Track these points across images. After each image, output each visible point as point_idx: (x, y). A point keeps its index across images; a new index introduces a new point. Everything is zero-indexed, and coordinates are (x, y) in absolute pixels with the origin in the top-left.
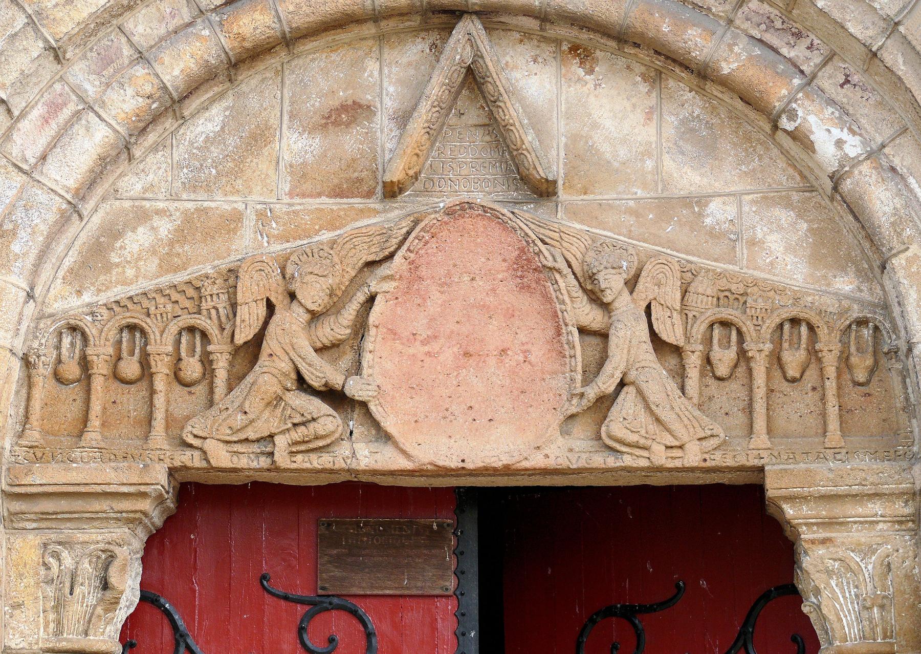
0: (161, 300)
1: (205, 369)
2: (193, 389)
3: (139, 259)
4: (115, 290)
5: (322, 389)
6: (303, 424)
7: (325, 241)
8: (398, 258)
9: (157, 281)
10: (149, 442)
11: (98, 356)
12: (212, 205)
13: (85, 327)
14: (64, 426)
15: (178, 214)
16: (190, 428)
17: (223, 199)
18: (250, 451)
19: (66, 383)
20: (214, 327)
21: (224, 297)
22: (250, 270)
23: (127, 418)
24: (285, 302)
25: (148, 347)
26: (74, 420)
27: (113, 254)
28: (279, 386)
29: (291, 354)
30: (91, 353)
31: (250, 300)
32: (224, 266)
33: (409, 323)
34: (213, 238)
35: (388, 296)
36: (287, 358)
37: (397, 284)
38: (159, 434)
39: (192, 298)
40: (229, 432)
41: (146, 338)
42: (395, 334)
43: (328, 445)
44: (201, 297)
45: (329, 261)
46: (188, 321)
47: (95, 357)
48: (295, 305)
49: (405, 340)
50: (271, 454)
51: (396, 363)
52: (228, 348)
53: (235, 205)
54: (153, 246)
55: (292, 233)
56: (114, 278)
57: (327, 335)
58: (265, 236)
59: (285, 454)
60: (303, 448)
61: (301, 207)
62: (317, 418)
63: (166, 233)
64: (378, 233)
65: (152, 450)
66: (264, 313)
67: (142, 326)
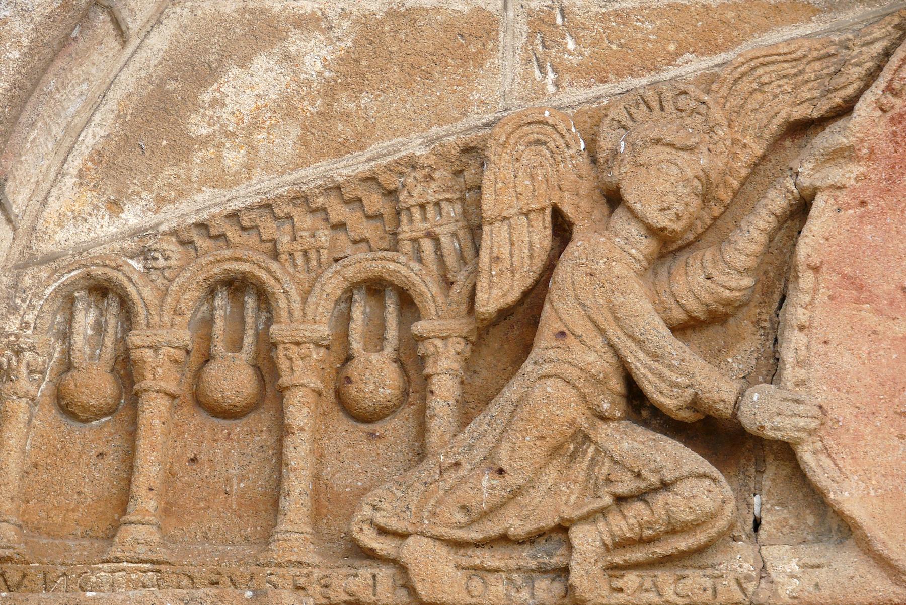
0: (304, 221)
1: (408, 380)
2: (378, 428)
3: (254, 126)
4: (199, 198)
5: (686, 415)
6: (641, 496)
7: (691, 77)
8: (864, 109)
9: (295, 175)
10: (272, 546)
11: (155, 348)
13: (126, 283)
14: (76, 516)
15: (346, 24)
16: (367, 511)
18: (512, 564)
19: (83, 416)
20: (428, 279)
21: (452, 211)
22: (512, 141)
23: (222, 497)
24: (597, 215)
25: (274, 328)
26: (99, 500)
27: (194, 118)
28: (582, 408)
29: (610, 332)
30: (140, 343)
31: (513, 211)
32: (452, 138)
33: (893, 264)
34: (428, 75)
35: (843, 197)
36: (599, 343)
37: (863, 169)
38: (296, 528)
39: (377, 217)
40: (460, 517)
41: (269, 311)
42: (860, 288)
43: (700, 550)
44: (398, 213)
45: (699, 119)
47: (149, 353)
48: (620, 218)
49: (883, 304)
50: (564, 571)
51: (865, 356)
52: (460, 325)
54: (288, 99)
56: (196, 172)
57: (696, 289)
59: (597, 570)
60: (639, 555)
62: (674, 482)
63: (319, 67)
64: (815, 54)
65: (279, 565)
66: (547, 243)
67: (258, 278)
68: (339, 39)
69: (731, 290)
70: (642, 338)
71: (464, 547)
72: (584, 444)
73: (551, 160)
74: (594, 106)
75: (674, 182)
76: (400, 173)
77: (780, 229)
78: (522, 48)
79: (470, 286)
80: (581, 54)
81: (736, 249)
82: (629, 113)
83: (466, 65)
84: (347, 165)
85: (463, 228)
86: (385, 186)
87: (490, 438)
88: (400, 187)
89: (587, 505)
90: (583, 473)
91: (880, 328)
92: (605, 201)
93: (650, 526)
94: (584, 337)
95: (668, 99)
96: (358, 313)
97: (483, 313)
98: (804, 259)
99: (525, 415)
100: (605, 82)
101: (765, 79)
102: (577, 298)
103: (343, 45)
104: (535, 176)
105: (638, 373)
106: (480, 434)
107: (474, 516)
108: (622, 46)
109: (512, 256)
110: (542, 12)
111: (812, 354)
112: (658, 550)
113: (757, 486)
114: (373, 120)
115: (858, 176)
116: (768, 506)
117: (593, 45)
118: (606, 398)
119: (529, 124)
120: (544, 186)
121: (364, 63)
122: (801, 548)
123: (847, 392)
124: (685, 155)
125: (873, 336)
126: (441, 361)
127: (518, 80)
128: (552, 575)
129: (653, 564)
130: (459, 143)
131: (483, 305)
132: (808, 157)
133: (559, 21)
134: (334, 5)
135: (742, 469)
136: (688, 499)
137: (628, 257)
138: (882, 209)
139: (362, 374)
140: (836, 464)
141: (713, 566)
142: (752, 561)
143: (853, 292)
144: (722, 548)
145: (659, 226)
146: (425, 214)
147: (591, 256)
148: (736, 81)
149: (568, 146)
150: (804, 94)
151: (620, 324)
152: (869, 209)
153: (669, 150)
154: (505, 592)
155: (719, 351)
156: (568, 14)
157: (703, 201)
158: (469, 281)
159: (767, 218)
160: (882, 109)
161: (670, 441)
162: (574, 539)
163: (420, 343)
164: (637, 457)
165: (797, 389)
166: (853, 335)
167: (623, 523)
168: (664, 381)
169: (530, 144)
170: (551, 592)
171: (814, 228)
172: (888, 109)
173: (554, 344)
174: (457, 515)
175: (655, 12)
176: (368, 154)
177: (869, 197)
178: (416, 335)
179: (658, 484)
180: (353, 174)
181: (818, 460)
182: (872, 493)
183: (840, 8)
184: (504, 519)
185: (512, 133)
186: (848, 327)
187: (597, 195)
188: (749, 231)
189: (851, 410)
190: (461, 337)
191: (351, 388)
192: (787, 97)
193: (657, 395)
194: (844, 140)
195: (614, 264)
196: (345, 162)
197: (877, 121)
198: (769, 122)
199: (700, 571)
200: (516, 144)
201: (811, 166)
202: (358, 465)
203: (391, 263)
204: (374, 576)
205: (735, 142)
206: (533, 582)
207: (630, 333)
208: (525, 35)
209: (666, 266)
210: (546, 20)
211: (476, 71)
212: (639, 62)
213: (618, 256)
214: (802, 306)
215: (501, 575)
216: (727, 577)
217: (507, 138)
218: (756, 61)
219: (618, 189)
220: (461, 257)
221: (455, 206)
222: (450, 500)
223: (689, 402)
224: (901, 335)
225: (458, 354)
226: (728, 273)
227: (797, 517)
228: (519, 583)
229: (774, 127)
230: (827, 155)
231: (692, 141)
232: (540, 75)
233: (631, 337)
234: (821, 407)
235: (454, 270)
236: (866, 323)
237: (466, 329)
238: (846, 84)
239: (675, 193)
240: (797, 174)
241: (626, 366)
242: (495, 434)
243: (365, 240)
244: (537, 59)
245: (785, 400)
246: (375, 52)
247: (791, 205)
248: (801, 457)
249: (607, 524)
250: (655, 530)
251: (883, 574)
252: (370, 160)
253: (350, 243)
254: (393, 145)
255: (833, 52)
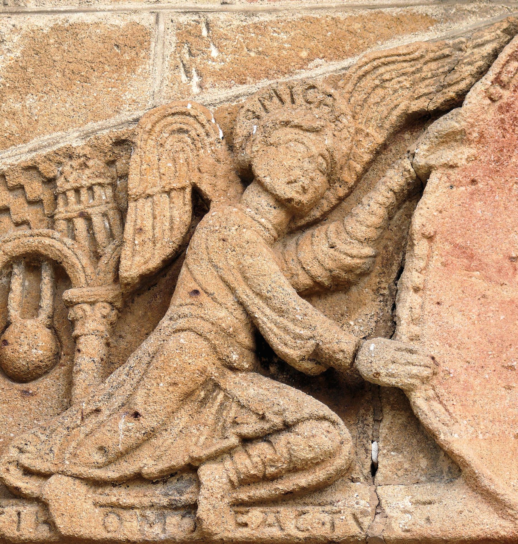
2: (31, 386)
5: (307, 366)
12: (88, 18)
15: (16, 38)
16: (14, 453)
17: (110, 7)
18: (146, 501)
20: (79, 252)
22: (157, 129)
24: (232, 192)
28: (213, 358)
31: (156, 190)
32: (106, 132)
33: (501, 236)
34: (87, 80)
35: (455, 175)
36: (230, 300)
37: (474, 151)
40: (99, 458)
42: (471, 257)
44: (56, 198)
45: (326, 109)
46: (25, 240)
48: (252, 189)
49: (492, 272)
50: (192, 507)
53: (135, 18)
55: (251, 66)
58: (194, 73)
61: (273, 17)
64: (432, 55)
66: (187, 217)
68: (9, 51)
69: (353, 257)
70: (268, 295)
71: (102, 486)
72: (214, 391)
73: (193, 146)
74: (235, 103)
75: (301, 158)
76: (58, 163)
77: (399, 208)
78: (170, 56)
79: (116, 257)
80: (223, 61)
81: (357, 221)
82: (263, 105)
83: (121, 70)
84: (11, 155)
85: (113, 208)
86: (45, 174)
87: (127, 387)
88: (59, 175)
89: (213, 445)
90: (212, 417)
91: (488, 293)
92: (240, 180)
93: (273, 464)
94: (216, 295)
95: (299, 92)
96: (17, 284)
97: (126, 278)
98: (419, 229)
99: (160, 364)
100: (244, 83)
101: (387, 76)
102: (210, 261)
103: (13, 56)
104: (177, 160)
105: (264, 327)
106: (119, 383)
107: (111, 456)
108: (259, 53)
109: (154, 229)
110: (190, 25)
111: (426, 313)
112: (280, 487)
113: (375, 434)
114: (36, 118)
115: (469, 157)
116: (385, 451)
117: (234, 52)
118: (235, 350)
119: (173, 114)
120: (186, 169)
121: (30, 70)
122: (414, 487)
123: (458, 348)
124: (312, 136)
125: (482, 300)
126: (88, 323)
127: (166, 82)
128: (183, 512)
129: (277, 502)
130: (111, 136)
131: (126, 271)
132: (424, 140)
133: (205, 33)
134: (6, 22)
135: (361, 419)
136: (308, 438)
137: (258, 225)
138: (491, 187)
139: (18, 337)
140: (447, 410)
141: (332, 504)
142: (369, 499)
143: (465, 260)
144: (341, 487)
145: (286, 197)
146: (79, 197)
147: (224, 224)
148: (360, 78)
149: (207, 135)
150: (421, 90)
151: (249, 283)
152: (478, 187)
153: (297, 131)
154: (139, 528)
155: (342, 315)
156: (213, 27)
157: (329, 181)
158: (115, 253)
159: (386, 194)
160: (491, 99)
161: (294, 389)
162: (202, 477)
163: (70, 309)
164: (261, 401)
165: (412, 343)
166: (464, 298)
167: (247, 462)
168: (288, 334)
169: (173, 132)
170: (181, 527)
171: (428, 202)
172: (496, 99)
173: (188, 301)
174: (95, 455)
175: (290, 25)
176: (31, 145)
177: (479, 176)
178: (66, 300)
179: (281, 426)
180: (16, 163)
181: (430, 406)
182: (481, 436)
183: (455, 19)
184: (138, 459)
185: (157, 122)
186: (460, 291)
187: (232, 176)
188: (369, 205)
189: (462, 363)
190: (107, 302)
191: (7, 350)
192: (406, 93)
193: (282, 347)
194: (457, 125)
195: (245, 230)
196: (9, 152)
197: (486, 108)
198: (389, 113)
199: (320, 507)
200: (161, 132)
201: (426, 147)
202: (11, 419)
203: (47, 238)
204: (19, 514)
205: (358, 131)
206: (165, 518)
207: (258, 291)
208: (174, 45)
209: (295, 239)
210: (192, 32)
211: (129, 75)
212: (275, 67)
213: (248, 224)
214: (417, 270)
215: (136, 512)
216: (344, 512)
217: (153, 126)
218: (378, 61)
219: (250, 166)
220: (111, 236)
221: (107, 190)
222: (89, 442)
223: (311, 352)
224: (509, 299)
225: (104, 317)
226: (350, 242)
227: (411, 460)
228: (152, 519)
229: (394, 117)
230: (441, 138)
231: (317, 124)
232: (186, 78)
233: (259, 294)
234: (433, 358)
235: (104, 245)
236: (476, 288)
237: (111, 296)
238: (459, 80)
239: (301, 168)
240: (414, 155)
241: (254, 321)
242: (132, 382)
243: (25, 223)
244: (184, 65)
245: (399, 349)
246: (40, 61)
247: (409, 184)
248: (414, 402)
249: (234, 463)
250: (277, 468)
251: (490, 508)
252: (31, 151)
253: (13, 226)
254: (53, 138)
255: (447, 53)
